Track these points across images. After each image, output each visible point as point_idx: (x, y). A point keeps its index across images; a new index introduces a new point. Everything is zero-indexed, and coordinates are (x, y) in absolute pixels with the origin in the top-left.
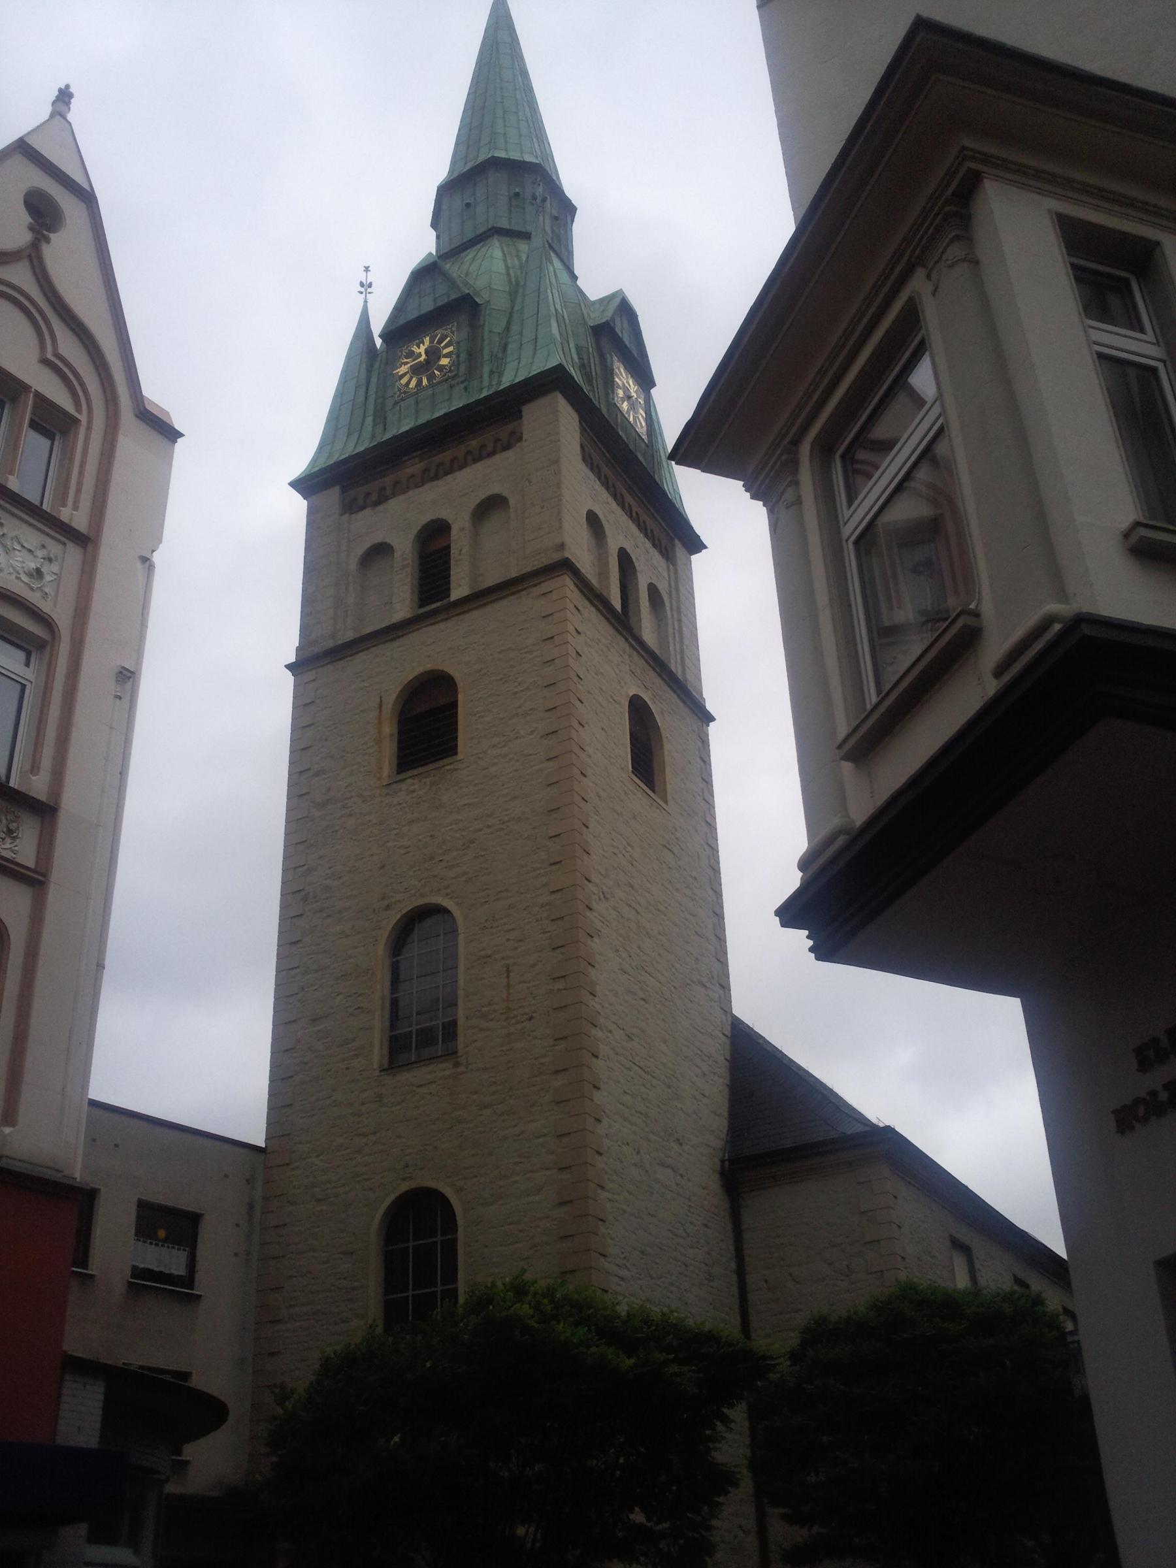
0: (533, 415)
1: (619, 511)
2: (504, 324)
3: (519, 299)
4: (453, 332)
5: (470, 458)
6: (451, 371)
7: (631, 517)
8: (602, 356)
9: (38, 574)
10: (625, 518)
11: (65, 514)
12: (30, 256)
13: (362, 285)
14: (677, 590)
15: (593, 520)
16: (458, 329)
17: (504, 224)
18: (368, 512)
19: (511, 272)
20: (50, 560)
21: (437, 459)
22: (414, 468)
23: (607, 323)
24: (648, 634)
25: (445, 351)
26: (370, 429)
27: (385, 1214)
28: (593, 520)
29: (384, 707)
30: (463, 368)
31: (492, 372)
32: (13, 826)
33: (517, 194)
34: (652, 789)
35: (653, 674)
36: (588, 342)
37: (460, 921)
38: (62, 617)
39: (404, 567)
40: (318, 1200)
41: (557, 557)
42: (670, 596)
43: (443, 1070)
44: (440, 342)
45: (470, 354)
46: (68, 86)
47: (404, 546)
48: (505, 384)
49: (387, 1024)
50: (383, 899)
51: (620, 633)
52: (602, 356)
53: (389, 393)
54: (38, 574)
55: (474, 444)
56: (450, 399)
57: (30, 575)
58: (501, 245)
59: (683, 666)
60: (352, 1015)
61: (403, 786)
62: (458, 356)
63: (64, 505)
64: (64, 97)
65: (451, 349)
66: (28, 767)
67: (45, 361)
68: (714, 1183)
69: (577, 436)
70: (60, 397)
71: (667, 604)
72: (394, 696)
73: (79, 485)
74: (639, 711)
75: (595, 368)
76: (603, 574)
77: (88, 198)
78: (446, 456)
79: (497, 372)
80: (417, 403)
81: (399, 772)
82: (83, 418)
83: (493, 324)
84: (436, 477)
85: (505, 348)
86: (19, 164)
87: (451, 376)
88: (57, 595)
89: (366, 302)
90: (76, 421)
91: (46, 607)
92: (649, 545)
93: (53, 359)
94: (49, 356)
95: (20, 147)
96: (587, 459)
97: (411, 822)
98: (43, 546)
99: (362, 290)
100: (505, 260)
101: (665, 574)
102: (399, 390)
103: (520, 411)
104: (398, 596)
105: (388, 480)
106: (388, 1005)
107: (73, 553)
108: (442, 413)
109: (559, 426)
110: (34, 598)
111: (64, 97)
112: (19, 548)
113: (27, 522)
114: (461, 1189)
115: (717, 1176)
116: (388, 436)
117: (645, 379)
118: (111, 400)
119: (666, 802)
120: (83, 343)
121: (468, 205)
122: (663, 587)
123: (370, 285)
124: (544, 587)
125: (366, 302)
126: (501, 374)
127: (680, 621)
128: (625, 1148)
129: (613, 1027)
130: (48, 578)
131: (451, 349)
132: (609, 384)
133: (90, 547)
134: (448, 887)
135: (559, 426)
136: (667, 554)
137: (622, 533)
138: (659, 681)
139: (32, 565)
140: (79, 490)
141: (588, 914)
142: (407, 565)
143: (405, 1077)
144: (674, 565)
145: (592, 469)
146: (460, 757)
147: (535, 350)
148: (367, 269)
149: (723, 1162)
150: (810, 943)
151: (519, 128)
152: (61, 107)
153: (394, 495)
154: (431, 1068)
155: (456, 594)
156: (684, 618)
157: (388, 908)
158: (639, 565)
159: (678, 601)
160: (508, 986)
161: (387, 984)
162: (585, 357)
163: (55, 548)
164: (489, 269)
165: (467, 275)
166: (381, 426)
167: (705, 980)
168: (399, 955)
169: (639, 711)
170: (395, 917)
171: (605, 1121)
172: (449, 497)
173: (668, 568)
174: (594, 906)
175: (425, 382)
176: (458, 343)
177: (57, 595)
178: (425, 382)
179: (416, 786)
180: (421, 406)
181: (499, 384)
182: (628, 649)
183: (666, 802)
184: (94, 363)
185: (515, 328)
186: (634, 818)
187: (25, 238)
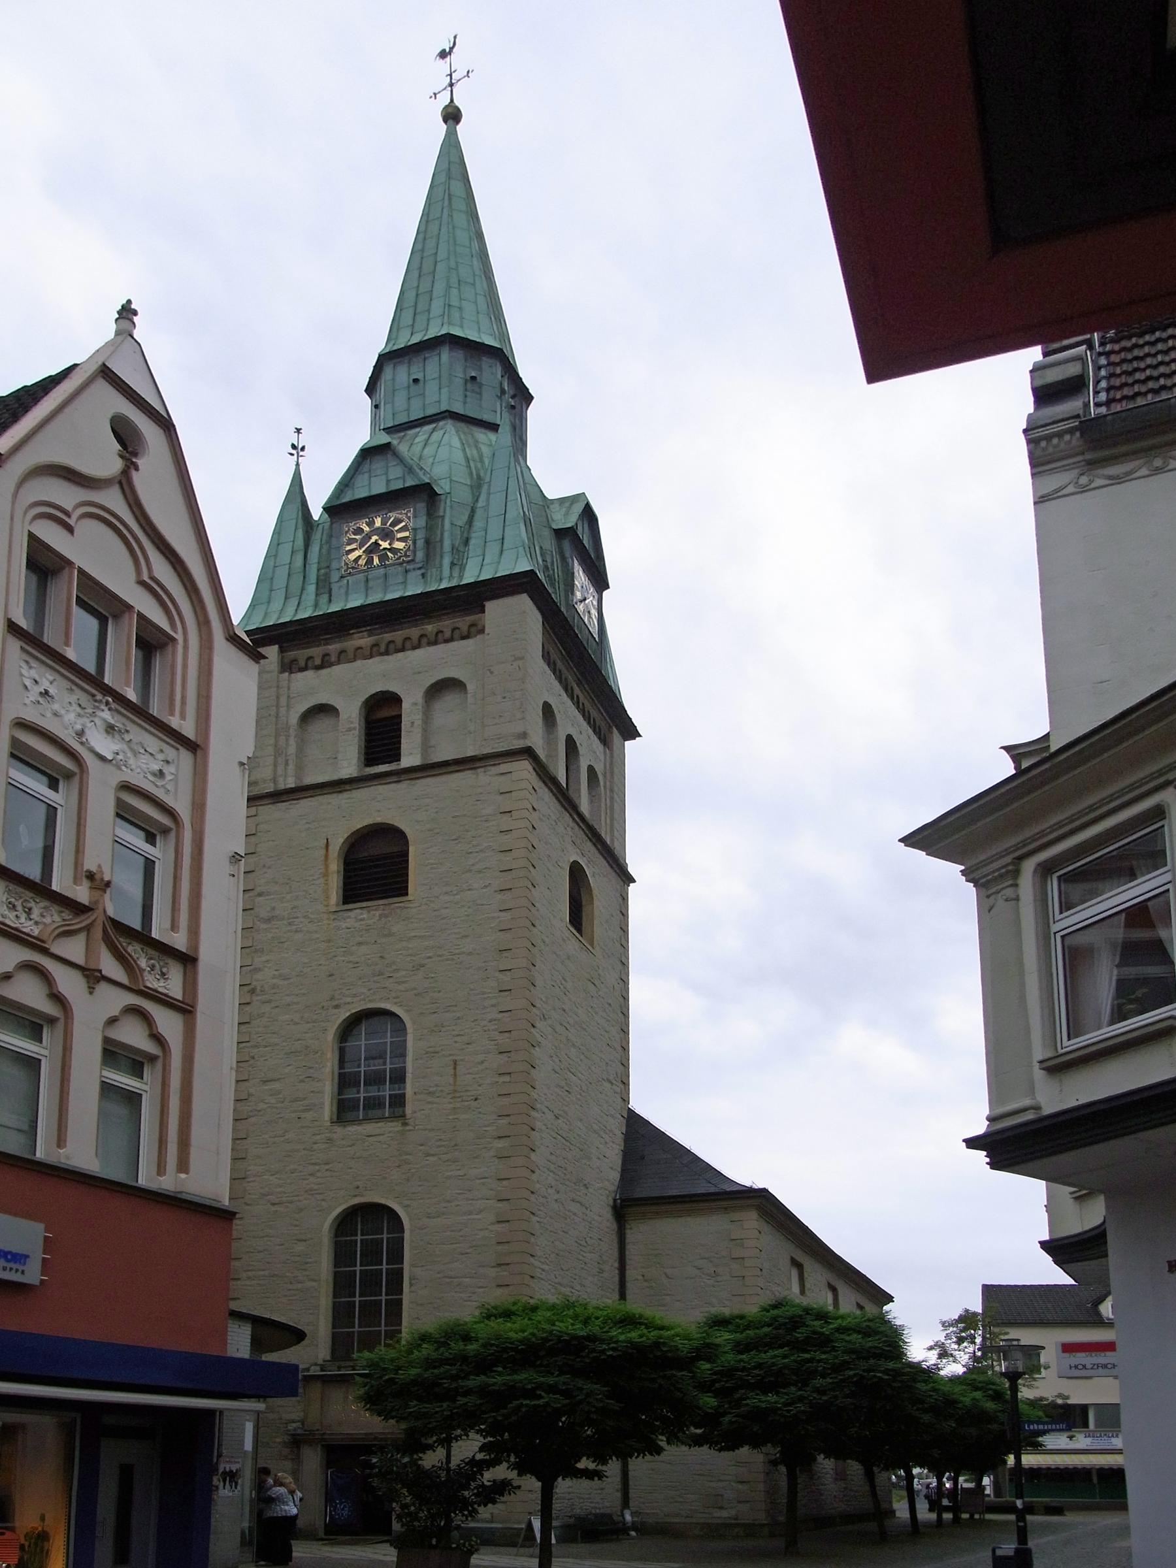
0: (495, 610)
1: (569, 703)
2: (465, 518)
3: (483, 498)
4: (409, 518)
5: (424, 640)
6: (405, 555)
7: (578, 708)
8: (563, 558)
9: (161, 774)
10: (573, 708)
11: (175, 722)
12: (120, 483)
13: (294, 447)
14: (612, 773)
15: (547, 710)
16: (415, 517)
17: (458, 408)
18: (309, 674)
19: (472, 465)
20: (168, 762)
21: (388, 637)
22: (362, 640)
23: (572, 528)
24: (585, 807)
25: (399, 535)
26: (313, 597)
27: (338, 1216)
28: (547, 710)
29: (330, 848)
30: (420, 555)
31: (453, 564)
32: (164, 970)
33: (473, 378)
34: (579, 930)
35: (589, 844)
36: (549, 543)
37: (409, 1024)
38: (182, 807)
39: (350, 730)
40: (273, 1204)
41: (519, 744)
42: (605, 776)
43: (394, 1127)
44: (394, 524)
45: (428, 542)
46: (129, 302)
47: (351, 712)
48: (468, 579)
49: (336, 1090)
50: (332, 999)
51: (566, 809)
52: (563, 558)
53: (334, 565)
54: (161, 774)
55: (430, 628)
56: (405, 583)
57: (154, 775)
58: (457, 432)
59: (612, 836)
60: (302, 1081)
61: (352, 914)
62: (415, 543)
63: (172, 714)
64: (127, 312)
65: (407, 534)
66: (168, 925)
67: (142, 583)
68: (608, 1214)
69: (540, 635)
70: (157, 617)
71: (602, 783)
72: (341, 840)
73: (183, 698)
74: (576, 872)
75: (558, 572)
76: (552, 755)
77: (166, 425)
78: (398, 635)
79: (458, 564)
80: (367, 580)
81: (344, 903)
82: (179, 637)
83: (452, 517)
84: (387, 653)
85: (466, 542)
86: (103, 388)
87: (405, 562)
88: (176, 790)
89: (298, 465)
90: (173, 640)
91: (169, 801)
92: (590, 731)
93: (149, 581)
94: (146, 578)
95: (102, 371)
96: (546, 656)
97: (360, 944)
98: (162, 751)
99: (294, 452)
100: (464, 450)
101: (602, 758)
102: (346, 564)
103: (484, 606)
104: (344, 754)
105: (333, 648)
106: (336, 1081)
107: (185, 756)
108: (396, 595)
109: (515, 619)
110: (159, 794)
111: (127, 312)
112: (142, 751)
113: (146, 730)
114: (408, 1206)
115: (609, 1209)
116: (334, 608)
117: (600, 582)
118: (203, 622)
119: (592, 945)
120: (179, 576)
121: (416, 381)
122: (599, 768)
123: (303, 449)
124: (504, 768)
125: (298, 465)
126: (462, 568)
127: (612, 798)
128: (550, 1191)
129: (546, 1110)
130: (169, 777)
131: (407, 534)
132: (570, 587)
133: (199, 752)
134: (397, 997)
135: (515, 619)
136: (605, 741)
137: (571, 722)
138: (593, 849)
139: (156, 767)
140: (183, 703)
141: (532, 1030)
142: (354, 729)
143: (352, 1129)
144: (611, 749)
145: (549, 665)
146: (410, 897)
147: (502, 551)
148: (298, 431)
149: (615, 1200)
150: (988, 1160)
151: (476, 303)
152: (125, 324)
153: (339, 662)
154: (380, 1125)
155: (406, 761)
156: (616, 796)
157: (337, 1007)
158: (582, 750)
159: (612, 782)
160: (455, 1075)
161: (336, 1062)
162: (549, 560)
163: (171, 753)
164: (441, 455)
165: (420, 458)
166: (326, 597)
167: (611, 1078)
168: (346, 1041)
169: (576, 872)
170: (344, 1014)
171: (537, 1171)
172: (404, 672)
173: (605, 752)
174: (537, 1025)
175: (376, 561)
176: (415, 530)
177: (176, 790)
178: (376, 561)
179: (364, 915)
180: (371, 584)
181: (461, 577)
182: (572, 824)
183: (592, 945)
184: (186, 588)
185: (478, 524)
186: (569, 958)
187: (117, 465)
